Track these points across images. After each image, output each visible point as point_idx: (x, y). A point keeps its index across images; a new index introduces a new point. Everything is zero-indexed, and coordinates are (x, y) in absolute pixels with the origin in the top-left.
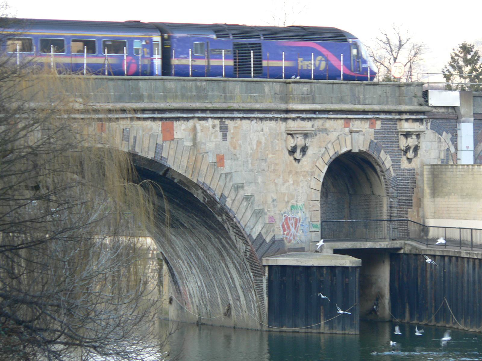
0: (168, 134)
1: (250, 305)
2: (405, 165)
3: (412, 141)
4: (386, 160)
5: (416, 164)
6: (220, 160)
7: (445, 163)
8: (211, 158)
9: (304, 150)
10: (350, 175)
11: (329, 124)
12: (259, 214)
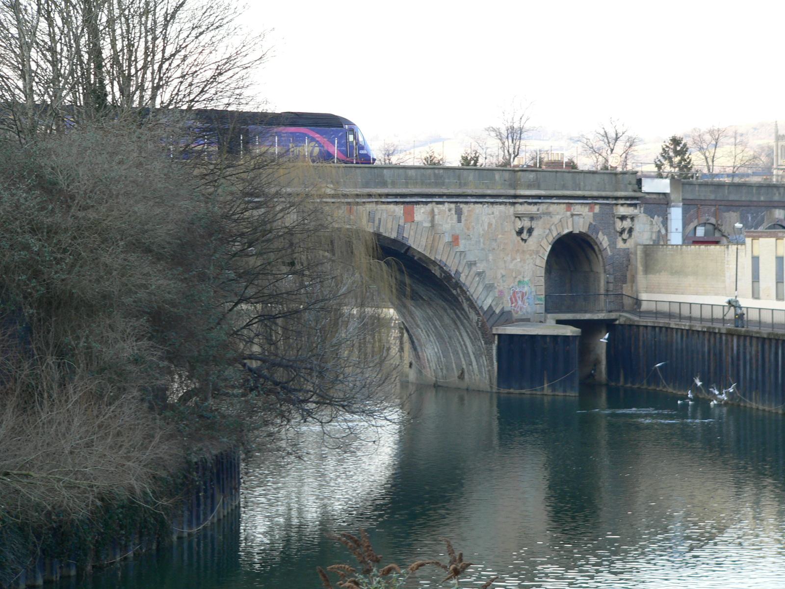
0: (409, 216)
1: (482, 370)
2: (620, 245)
3: (627, 224)
4: (603, 240)
5: (630, 244)
6: (455, 240)
7: (656, 243)
8: (447, 238)
9: (530, 231)
10: (571, 255)
11: (552, 208)
12: (489, 288)
